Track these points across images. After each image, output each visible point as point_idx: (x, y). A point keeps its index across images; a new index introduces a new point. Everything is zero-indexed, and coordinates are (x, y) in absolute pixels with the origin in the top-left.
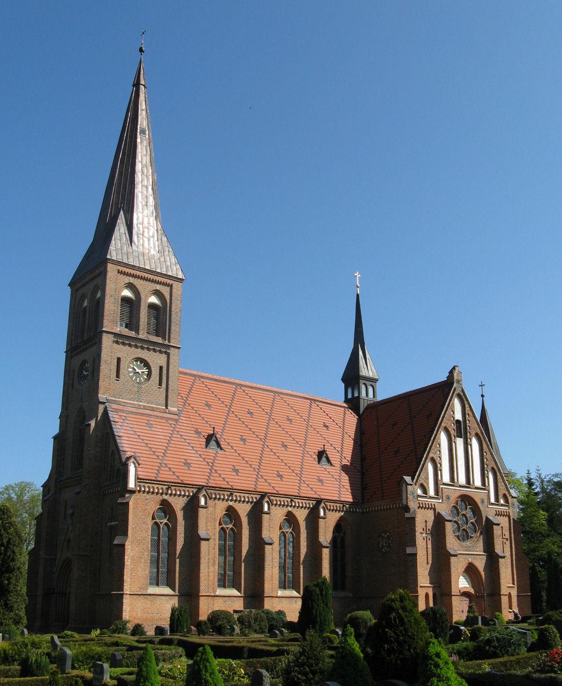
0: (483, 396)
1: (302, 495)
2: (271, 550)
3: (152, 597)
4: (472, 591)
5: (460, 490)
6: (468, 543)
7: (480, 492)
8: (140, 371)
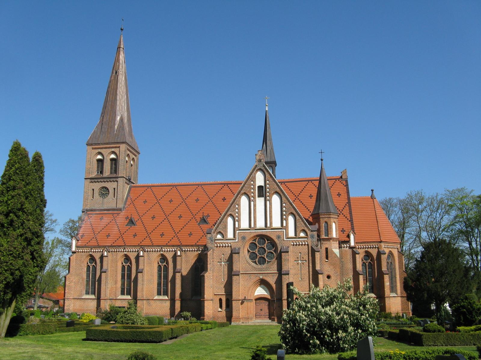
0: (322, 160)
1: (99, 245)
2: (141, 276)
3: (84, 300)
4: (269, 297)
5: (255, 232)
6: (265, 265)
7: (276, 231)
8: (105, 193)
